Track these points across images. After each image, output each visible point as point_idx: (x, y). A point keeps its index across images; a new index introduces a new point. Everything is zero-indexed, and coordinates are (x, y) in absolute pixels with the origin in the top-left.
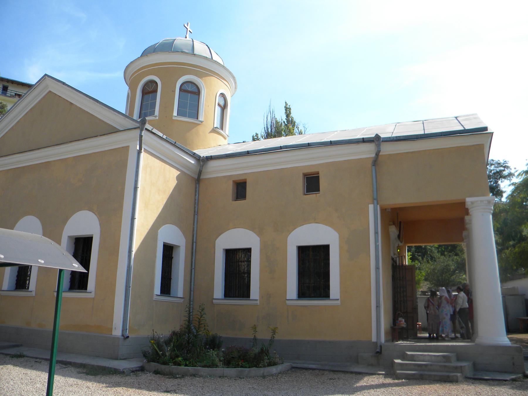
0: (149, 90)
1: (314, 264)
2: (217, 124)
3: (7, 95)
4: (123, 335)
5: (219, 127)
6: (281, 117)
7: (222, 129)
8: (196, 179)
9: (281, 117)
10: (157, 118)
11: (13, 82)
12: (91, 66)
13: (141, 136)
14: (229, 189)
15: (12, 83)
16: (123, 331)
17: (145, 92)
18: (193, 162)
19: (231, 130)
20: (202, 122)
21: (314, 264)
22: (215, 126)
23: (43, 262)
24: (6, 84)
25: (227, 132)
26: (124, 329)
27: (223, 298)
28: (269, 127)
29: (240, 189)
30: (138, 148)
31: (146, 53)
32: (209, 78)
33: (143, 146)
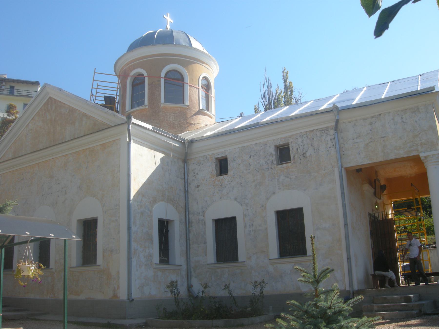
0: (138, 82)
1: (291, 230)
2: (202, 106)
3: (15, 94)
4: (128, 299)
5: (205, 109)
6: (278, 85)
7: (208, 110)
8: (182, 159)
9: (278, 85)
10: (147, 107)
11: (18, 82)
12: (82, 72)
13: (129, 130)
14: (211, 168)
15: (18, 83)
16: (128, 295)
17: (134, 85)
18: (178, 145)
19: (224, 103)
20: (188, 106)
21: (291, 230)
22: (201, 108)
23: (53, 235)
24: (13, 84)
25: (213, 112)
26: (129, 294)
27: (158, 263)
28: (266, 94)
29: (223, 166)
30: (128, 140)
31: (133, 47)
32: (194, 65)
33: (132, 137)
